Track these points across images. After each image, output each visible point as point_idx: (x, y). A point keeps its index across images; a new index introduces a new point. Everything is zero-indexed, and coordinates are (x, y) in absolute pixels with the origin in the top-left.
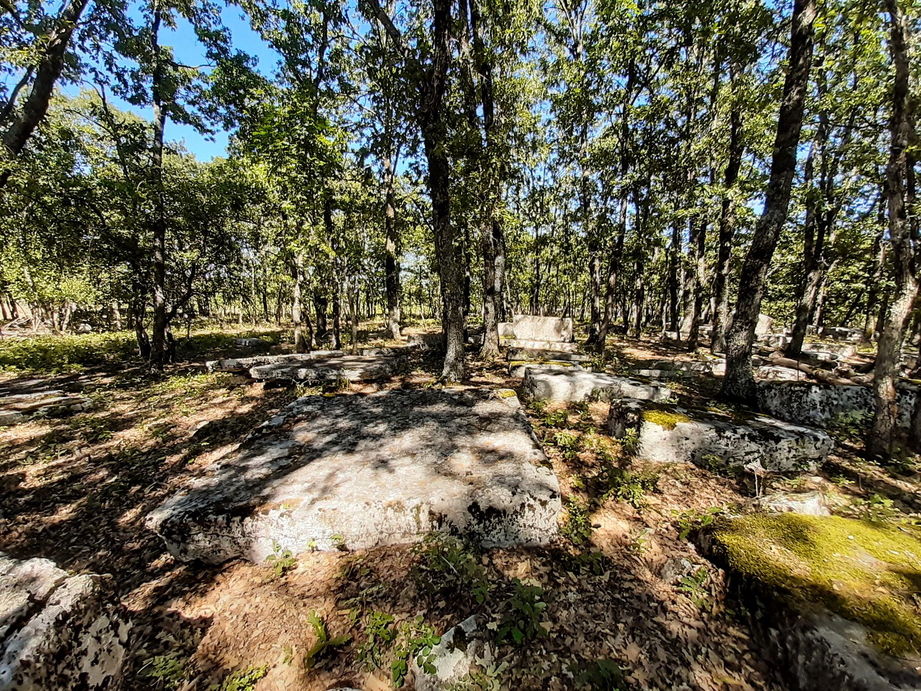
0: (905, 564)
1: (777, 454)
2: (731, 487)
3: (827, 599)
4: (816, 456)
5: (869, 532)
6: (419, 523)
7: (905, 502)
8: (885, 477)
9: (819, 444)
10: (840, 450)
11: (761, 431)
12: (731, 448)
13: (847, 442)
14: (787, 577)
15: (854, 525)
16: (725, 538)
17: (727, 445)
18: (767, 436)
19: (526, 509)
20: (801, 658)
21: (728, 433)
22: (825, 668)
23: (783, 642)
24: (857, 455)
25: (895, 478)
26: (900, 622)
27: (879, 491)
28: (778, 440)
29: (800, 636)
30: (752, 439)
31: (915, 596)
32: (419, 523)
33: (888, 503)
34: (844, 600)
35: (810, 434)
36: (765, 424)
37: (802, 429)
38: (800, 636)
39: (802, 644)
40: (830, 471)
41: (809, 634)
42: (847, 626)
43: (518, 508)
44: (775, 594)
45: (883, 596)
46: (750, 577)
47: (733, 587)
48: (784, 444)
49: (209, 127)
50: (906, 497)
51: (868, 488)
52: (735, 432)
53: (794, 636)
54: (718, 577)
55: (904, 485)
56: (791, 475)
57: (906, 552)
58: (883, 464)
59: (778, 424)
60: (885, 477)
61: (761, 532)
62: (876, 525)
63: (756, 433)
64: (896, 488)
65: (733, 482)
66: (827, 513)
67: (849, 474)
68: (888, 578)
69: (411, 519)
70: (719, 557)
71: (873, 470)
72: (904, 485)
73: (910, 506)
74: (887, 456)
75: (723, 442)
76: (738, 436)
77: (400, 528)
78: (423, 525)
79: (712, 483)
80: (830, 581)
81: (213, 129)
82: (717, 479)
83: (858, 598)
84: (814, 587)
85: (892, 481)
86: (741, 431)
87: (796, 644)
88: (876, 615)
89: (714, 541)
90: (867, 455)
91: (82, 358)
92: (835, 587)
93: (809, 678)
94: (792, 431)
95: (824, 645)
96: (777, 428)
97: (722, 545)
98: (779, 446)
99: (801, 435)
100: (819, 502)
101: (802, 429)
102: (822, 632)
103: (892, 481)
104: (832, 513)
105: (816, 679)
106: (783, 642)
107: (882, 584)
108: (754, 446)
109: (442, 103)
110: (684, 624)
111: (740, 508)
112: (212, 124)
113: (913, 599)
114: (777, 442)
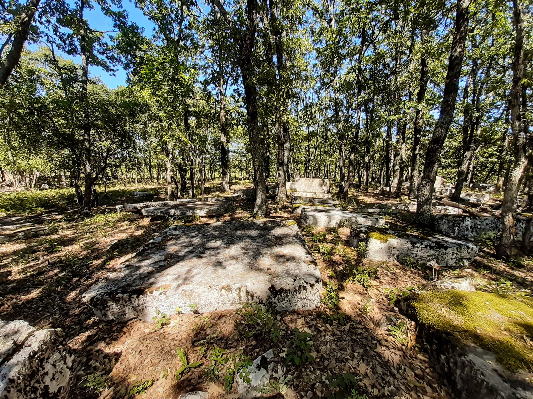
4: (468, 257)
5: (498, 300)
6: (240, 297)
7: (518, 283)
8: (507, 269)
9: (470, 250)
10: (481, 254)
11: (437, 243)
13: (486, 249)
15: (490, 296)
19: (302, 289)
20: (458, 372)
23: (448, 363)
25: (513, 269)
28: (446, 248)
29: (458, 359)
32: (240, 297)
33: (509, 283)
37: (460, 242)
38: (458, 359)
39: (459, 364)
43: (297, 288)
44: (444, 335)
45: (505, 337)
46: (430, 327)
48: (449, 250)
49: (112, 68)
55: (518, 273)
61: (436, 300)
63: (434, 245)
65: (420, 272)
66: (474, 289)
69: (236, 295)
72: (518, 273)
75: (416, 249)
76: (423, 246)
77: (229, 301)
78: (242, 299)
79: (409, 273)
80: (475, 328)
81: (115, 68)
82: (411, 271)
86: (426, 243)
87: (455, 363)
90: (497, 257)
92: (478, 331)
93: (463, 383)
94: (454, 243)
96: (446, 242)
99: (460, 245)
100: (469, 283)
101: (460, 242)
106: (448, 363)
107: (505, 330)
109: (253, 53)
111: (424, 287)
112: (114, 66)
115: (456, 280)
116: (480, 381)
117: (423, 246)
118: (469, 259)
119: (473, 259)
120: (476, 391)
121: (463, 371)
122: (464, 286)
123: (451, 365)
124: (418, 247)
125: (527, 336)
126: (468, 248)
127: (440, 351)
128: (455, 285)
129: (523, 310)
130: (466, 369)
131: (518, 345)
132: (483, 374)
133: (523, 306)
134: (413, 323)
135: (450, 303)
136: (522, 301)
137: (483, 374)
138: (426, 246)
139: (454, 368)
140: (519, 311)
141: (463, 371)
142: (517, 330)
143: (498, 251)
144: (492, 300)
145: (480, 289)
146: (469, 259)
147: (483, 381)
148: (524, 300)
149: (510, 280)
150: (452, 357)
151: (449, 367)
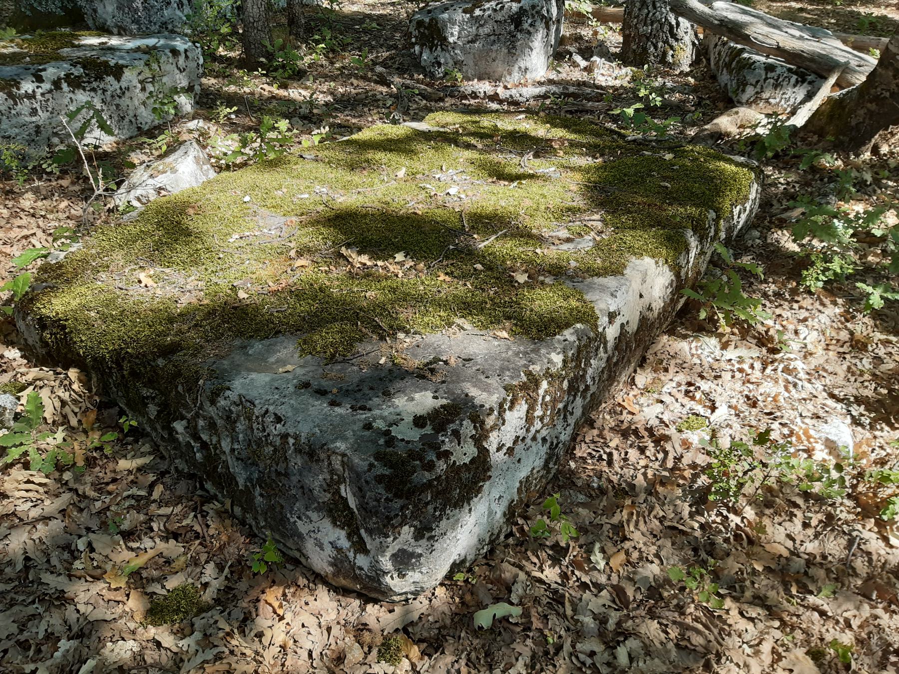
0: (321, 208)
1: (124, 102)
2: (64, 193)
3: (236, 323)
4: (184, 83)
5: (267, 178)
7: (304, 118)
8: (275, 90)
9: (181, 60)
10: (217, 66)
11: (87, 64)
12: (42, 117)
13: (221, 51)
14: (171, 320)
15: (247, 177)
16: (57, 305)
17: (34, 112)
18: (97, 70)
20: (226, 445)
21: (27, 86)
22: (259, 443)
23: (196, 437)
24: (239, 67)
25: (284, 86)
26: (336, 302)
27: (271, 113)
28: (118, 72)
29: (211, 411)
30: (76, 83)
31: (343, 250)
33: (283, 124)
34: (257, 308)
35: (164, 47)
36: (91, 46)
37: (151, 42)
38: (211, 411)
39: (220, 422)
40: (207, 103)
41: (222, 403)
42: (270, 350)
44: (161, 362)
45: (305, 270)
46: (119, 357)
47: (104, 390)
48: (130, 77)
50: (304, 110)
51: (254, 110)
52: (39, 79)
53: (205, 418)
54: (53, 392)
55: (296, 93)
56: (153, 132)
57: (318, 188)
58: (270, 71)
59: (114, 41)
60: (275, 90)
61: (118, 257)
62: (272, 165)
63: (78, 71)
64: (290, 101)
65: (65, 183)
66: (212, 174)
67: (230, 100)
68: (305, 240)
70: (54, 348)
71: (257, 86)
72: (296, 93)
73: (311, 122)
74: (270, 56)
75: (24, 107)
76: (47, 86)
79: (27, 201)
80: (234, 288)
82: (36, 191)
83: (275, 293)
84: (211, 313)
85: (282, 93)
86: (51, 72)
87: (212, 426)
88: (303, 307)
89: (43, 323)
90: (248, 64)
91: (678, 242)
92: (242, 295)
93: (245, 468)
94: (138, 49)
95: (245, 402)
96: (112, 49)
97: (58, 324)
98: (124, 84)
99: (148, 51)
100: (197, 159)
101: (151, 42)
102: (238, 386)
103: (282, 93)
104: (220, 169)
105: (254, 464)
106: (196, 437)
107: (300, 254)
108: (82, 97)
110: (34, 523)
111: (83, 228)
113: (342, 256)
114: (118, 78)
115: (160, 165)
116: (278, 441)
117: (47, 86)
118: (190, 89)
119: (197, 88)
120: (278, 474)
121: (235, 439)
122: (182, 174)
123: (205, 437)
124: (31, 96)
125: (348, 246)
126: (175, 52)
127: (167, 415)
128: (161, 180)
129: (322, 182)
130: (240, 427)
131: (332, 278)
132: (278, 419)
133: (322, 170)
134: (73, 373)
135: (159, 246)
136: (316, 160)
137: (278, 419)
138: (57, 84)
139: (215, 439)
140: (318, 188)
141: (235, 439)
142: (308, 236)
143: (247, 49)
144: (254, 187)
145: (228, 168)
146: (190, 89)
147: (285, 436)
148: (321, 154)
149: (285, 116)
150: (197, 415)
151: (204, 446)
